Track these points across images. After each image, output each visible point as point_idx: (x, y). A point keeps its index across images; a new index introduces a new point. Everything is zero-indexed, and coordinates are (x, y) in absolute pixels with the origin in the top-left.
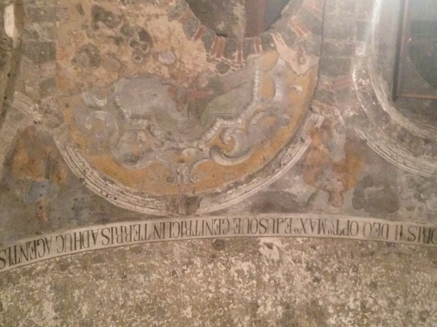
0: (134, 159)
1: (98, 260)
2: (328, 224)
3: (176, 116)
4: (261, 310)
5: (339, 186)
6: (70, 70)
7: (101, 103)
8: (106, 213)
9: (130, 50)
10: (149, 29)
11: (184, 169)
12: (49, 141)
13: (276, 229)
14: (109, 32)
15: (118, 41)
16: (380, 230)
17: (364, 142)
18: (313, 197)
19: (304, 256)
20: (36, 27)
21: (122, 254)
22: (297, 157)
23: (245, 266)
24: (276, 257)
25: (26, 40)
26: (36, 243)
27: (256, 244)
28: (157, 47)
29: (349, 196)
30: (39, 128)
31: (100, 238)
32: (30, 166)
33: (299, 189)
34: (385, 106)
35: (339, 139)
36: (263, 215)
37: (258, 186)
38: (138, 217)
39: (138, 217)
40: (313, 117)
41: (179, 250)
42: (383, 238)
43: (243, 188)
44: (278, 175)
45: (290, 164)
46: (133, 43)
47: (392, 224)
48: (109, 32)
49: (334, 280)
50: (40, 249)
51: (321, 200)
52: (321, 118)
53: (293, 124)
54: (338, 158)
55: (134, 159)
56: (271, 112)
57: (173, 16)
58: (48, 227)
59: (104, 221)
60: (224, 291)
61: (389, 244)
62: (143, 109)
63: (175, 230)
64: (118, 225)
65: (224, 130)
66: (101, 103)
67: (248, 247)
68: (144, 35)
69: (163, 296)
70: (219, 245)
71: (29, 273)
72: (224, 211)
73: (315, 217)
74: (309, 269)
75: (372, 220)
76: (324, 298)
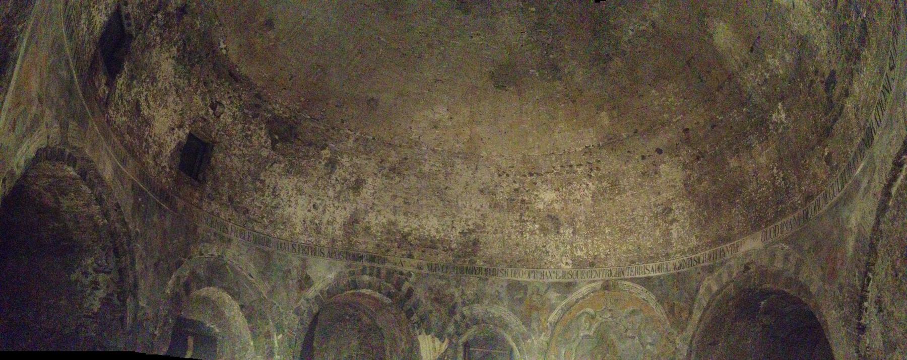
0: (633, 312)
1: (651, 258)
2: (539, 276)
3: (613, 337)
4: (571, 231)
5: (535, 298)
7: (649, 347)
8: (646, 282)
11: (609, 306)
12: (672, 324)
13: (564, 273)
18: (547, 291)
19: (550, 259)
21: (640, 260)
23: (579, 253)
26: (679, 268)
27: (574, 265)
29: (529, 292)
31: (650, 269)
32: (681, 310)
33: (553, 296)
35: (534, 325)
36: (572, 280)
38: (632, 280)
39: (632, 280)
41: (612, 262)
49: (536, 247)
50: (678, 265)
51: (543, 289)
52: (542, 338)
59: (649, 278)
60: (590, 241)
62: (629, 342)
63: (614, 272)
65: (589, 329)
67: (578, 264)
69: (620, 238)
70: (592, 265)
71: (683, 253)
72: (590, 282)
74: (548, 252)
75: (520, 279)
76: (540, 237)
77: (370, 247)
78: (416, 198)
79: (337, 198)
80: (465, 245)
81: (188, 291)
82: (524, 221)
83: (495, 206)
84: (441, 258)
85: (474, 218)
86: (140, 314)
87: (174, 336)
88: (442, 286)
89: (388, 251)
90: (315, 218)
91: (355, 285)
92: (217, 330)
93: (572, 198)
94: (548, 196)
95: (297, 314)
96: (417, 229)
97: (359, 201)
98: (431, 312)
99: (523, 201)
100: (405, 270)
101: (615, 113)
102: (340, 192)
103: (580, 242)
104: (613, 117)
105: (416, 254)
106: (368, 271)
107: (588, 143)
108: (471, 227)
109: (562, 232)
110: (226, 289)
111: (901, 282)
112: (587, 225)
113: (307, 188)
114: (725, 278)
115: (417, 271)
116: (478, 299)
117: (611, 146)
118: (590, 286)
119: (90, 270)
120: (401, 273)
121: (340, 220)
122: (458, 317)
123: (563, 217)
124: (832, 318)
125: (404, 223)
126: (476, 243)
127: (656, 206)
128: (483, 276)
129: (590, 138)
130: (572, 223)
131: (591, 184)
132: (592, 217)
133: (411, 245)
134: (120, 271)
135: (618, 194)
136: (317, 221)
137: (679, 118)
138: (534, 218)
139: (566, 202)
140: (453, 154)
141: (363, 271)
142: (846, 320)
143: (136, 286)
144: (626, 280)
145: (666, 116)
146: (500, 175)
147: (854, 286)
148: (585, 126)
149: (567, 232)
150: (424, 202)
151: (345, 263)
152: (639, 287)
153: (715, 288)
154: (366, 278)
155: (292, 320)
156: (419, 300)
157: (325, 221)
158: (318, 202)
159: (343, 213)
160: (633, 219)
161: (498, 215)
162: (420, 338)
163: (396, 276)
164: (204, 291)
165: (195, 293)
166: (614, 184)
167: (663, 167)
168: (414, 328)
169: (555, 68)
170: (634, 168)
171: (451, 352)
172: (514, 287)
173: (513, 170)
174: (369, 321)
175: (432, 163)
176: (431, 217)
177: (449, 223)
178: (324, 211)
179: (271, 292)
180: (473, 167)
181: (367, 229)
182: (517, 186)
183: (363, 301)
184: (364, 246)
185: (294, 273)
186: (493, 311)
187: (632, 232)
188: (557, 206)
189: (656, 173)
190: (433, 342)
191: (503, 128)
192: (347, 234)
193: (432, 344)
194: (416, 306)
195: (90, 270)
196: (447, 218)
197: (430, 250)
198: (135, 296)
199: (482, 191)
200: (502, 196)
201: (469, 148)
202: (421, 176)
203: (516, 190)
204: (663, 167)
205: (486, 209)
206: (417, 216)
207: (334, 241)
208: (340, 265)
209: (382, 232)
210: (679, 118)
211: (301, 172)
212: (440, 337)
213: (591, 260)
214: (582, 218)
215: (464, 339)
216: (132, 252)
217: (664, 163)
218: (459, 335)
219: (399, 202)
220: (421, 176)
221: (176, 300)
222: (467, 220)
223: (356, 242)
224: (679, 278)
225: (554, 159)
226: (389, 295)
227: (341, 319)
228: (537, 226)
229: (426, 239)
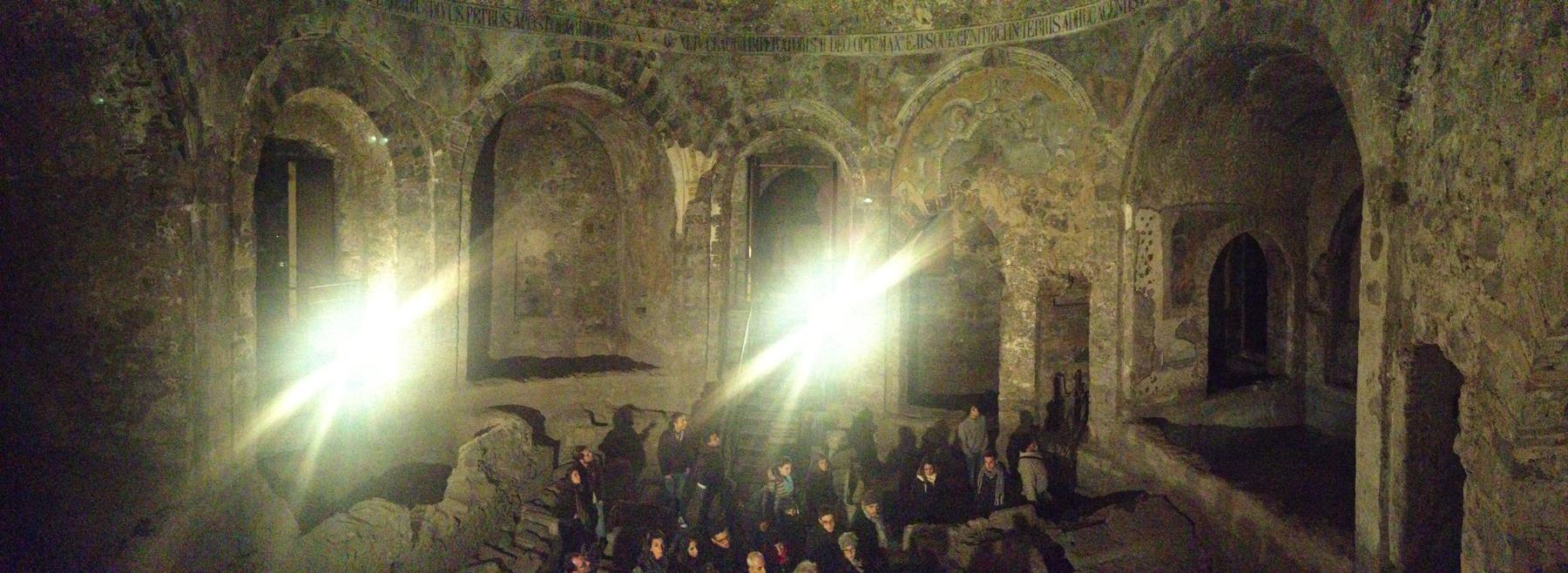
0: (1035, 101)
3: (1003, 142)
6: (1085, 178)
7: (1060, 152)
8: (1056, 48)
9: (1038, 197)
10: (1024, 215)
12: (1100, 115)
14: (1055, 212)
15: (1048, 205)
16: (838, 45)
17: (853, 124)
20: (1109, 213)
22: (905, 108)
24: (919, 10)
25: (1115, 202)
28: (1018, 200)
30: (1107, 127)
31: (1061, 23)
33: (903, 79)
34: (839, 156)
35: (873, 126)
37: (935, 79)
38: (1029, 45)
39: (1029, 45)
40: (894, 145)
42: (835, 38)
43: (947, 77)
44: (921, 89)
45: (910, 101)
46: (1036, 203)
47: (828, 52)
48: (1055, 212)
50: (1108, 11)
51: (884, 69)
52: (887, 143)
53: (910, 137)
54: (873, 109)
55: (1035, 101)
56: (927, 148)
57: (1006, 226)
58: (1103, 31)
59: (1058, 39)
61: (830, 33)
62: (1028, 148)
63: (1001, 31)
64: (1047, 36)
65: (964, 130)
66: (1060, 152)
67: (942, 19)
68: (1028, 210)
70: (966, 20)
72: (964, 53)
73: (888, 53)
81: (281, 99)
86: (206, 136)
87: (262, 165)
91: (558, 75)
92: (332, 151)
95: (467, 122)
100: (649, 46)
110: (343, 89)
111: (1481, 14)
114: (1187, 29)
116: (774, 90)
118: (963, 58)
119: (117, 84)
120: (639, 54)
122: (736, 120)
124: (1360, 86)
134: (165, 79)
142: (1382, 88)
143: (193, 96)
144: (1017, 45)
147: (1400, 30)
152: (1041, 56)
153: (1169, 49)
154: (579, 63)
155: (463, 135)
162: (671, 152)
164: (308, 96)
165: (292, 99)
168: (660, 138)
171: (722, 169)
174: (585, 133)
179: (423, 90)
183: (577, 103)
185: (461, 58)
186: (800, 108)
190: (693, 157)
193: (689, 160)
195: (117, 84)
198: (195, 113)
212: (705, 150)
215: (748, 151)
216: (177, 45)
218: (738, 146)
221: (262, 112)
224: (1109, 37)
226: (620, 91)
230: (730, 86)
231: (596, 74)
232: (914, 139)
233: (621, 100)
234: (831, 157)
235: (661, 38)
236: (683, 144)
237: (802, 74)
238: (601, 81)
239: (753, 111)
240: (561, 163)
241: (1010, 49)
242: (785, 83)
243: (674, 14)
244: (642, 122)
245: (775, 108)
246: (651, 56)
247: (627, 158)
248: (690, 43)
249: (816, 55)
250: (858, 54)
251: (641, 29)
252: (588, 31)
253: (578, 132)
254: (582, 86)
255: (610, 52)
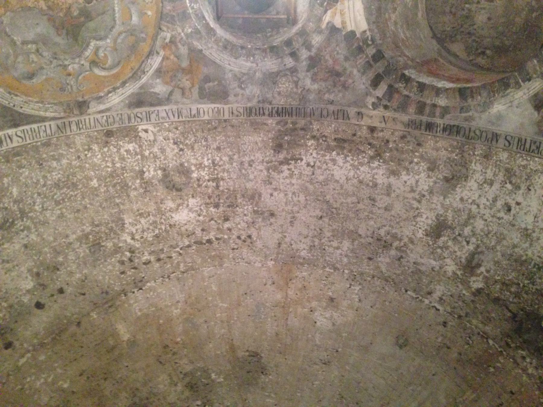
0: (31, 76)
1: (17, 154)
2: (184, 112)
4: (146, 174)
5: (187, 84)
13: (148, 119)
16: (219, 111)
18: (171, 94)
19: (171, 135)
21: (36, 149)
22: (155, 66)
23: (131, 147)
27: (136, 130)
29: (195, 91)
31: (15, 138)
33: (160, 88)
34: (212, 24)
35: (183, 50)
37: (131, 89)
38: (43, 119)
39: (43, 119)
40: (163, 34)
42: (221, 117)
43: (120, 91)
44: (144, 80)
45: (151, 72)
47: (226, 107)
49: (193, 148)
51: (177, 95)
52: (169, 35)
54: (185, 64)
59: (16, 125)
60: (118, 165)
61: (225, 121)
63: (74, 127)
64: (27, 127)
65: (97, 49)
67: (130, 133)
69: (74, 174)
70: (109, 134)
73: (174, 107)
74: (175, 143)
75: (213, 106)
76: (188, 161)
77: (431, 143)
78: (360, 206)
79: (471, 216)
80: (293, 144)
82: (213, 180)
83: (253, 197)
84: (329, 128)
85: (281, 178)
88: (329, 91)
89: (403, 137)
90: (511, 193)
91: (462, 93)
93: (152, 218)
94: (182, 217)
96: (361, 164)
97: (439, 207)
98: (346, 59)
99: (217, 206)
100: (380, 112)
101: (111, 342)
102: (466, 224)
103: (132, 163)
104: (112, 335)
105: (364, 132)
106: (438, 111)
107: (139, 294)
108: (285, 167)
109: (159, 172)
112: (125, 187)
113: (515, 237)
115: (363, 110)
116: (272, 78)
117: (110, 297)
118: (107, 106)
120: (386, 107)
121: (472, 184)
122: (304, 54)
123: (161, 191)
125: (379, 173)
126: (278, 148)
127: (28, 228)
128: (267, 106)
129: (138, 303)
130: (147, 185)
131: (129, 240)
132: (119, 197)
133: (370, 144)
135: (89, 234)
136: (509, 186)
137: (23, 361)
138: (199, 186)
139: (160, 212)
140: (311, 263)
141: (446, 111)
144: (54, 119)
145: (42, 358)
146: (250, 237)
148: (147, 316)
149: (152, 172)
150: (349, 200)
151: (474, 123)
156: (363, 74)
157: (496, 186)
158: (502, 214)
159: (466, 194)
160: (57, 203)
161: (249, 185)
162: (363, 25)
163: (395, 103)
166: (96, 246)
167: (29, 284)
169: (192, 387)
170: (71, 273)
172: (220, 95)
173: (233, 245)
175: (339, 252)
176: (343, 180)
177: (318, 172)
178: (495, 200)
180: (284, 246)
181: (432, 167)
182: (227, 225)
184: (439, 144)
186: (249, 64)
187: (57, 185)
188: (170, 204)
189: (38, 274)
190: (343, 23)
191: (249, 300)
192: (465, 165)
194: (369, 65)
196: (321, 178)
197: (344, 137)
199: (272, 215)
200: (246, 208)
201: (290, 271)
202: (353, 235)
203: (226, 219)
204: (29, 284)
205: (265, 191)
206: (361, 182)
207: (487, 156)
208: (481, 121)
209: (411, 162)
210: (23, 361)
211: (521, 262)
213: (113, 140)
214: (133, 194)
217: (28, 291)
219: (383, 201)
220: (353, 235)
222: (291, 176)
223: (453, 152)
225: (182, 265)
226: (407, 80)
227: (501, 50)
228: (195, 175)
229: (350, 151)
230: (308, 82)
231: (426, 93)
232: (144, 40)
233: (406, 72)
234: (221, 25)
235: (365, 118)
236: (353, 33)
237: (248, 92)
238: (422, 87)
239: (289, 62)
240: (481, 18)
241: (62, 114)
242: (263, 83)
243: (354, 135)
244: (388, 54)
245: (270, 64)
246: (375, 106)
247: (409, 22)
248: (344, 115)
249: (236, 104)
250: (199, 106)
251: (383, 125)
252: (430, 127)
253: (457, 48)
254: (441, 84)
255: (412, 109)
